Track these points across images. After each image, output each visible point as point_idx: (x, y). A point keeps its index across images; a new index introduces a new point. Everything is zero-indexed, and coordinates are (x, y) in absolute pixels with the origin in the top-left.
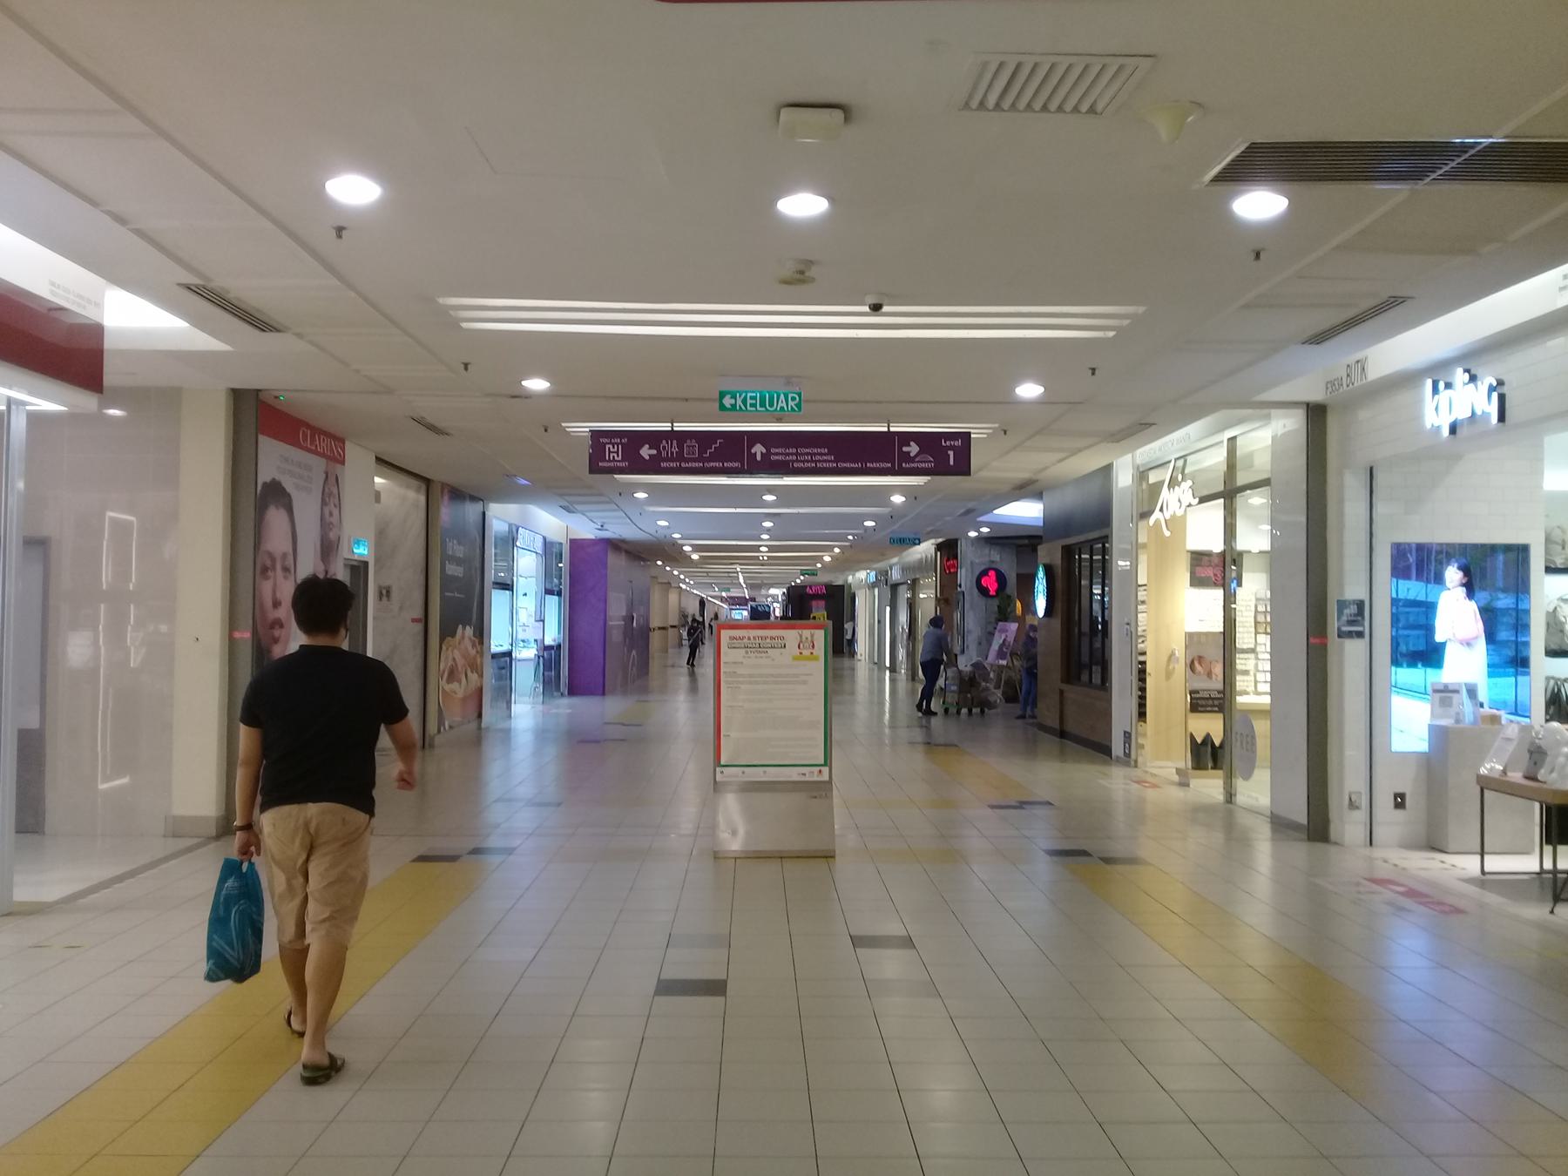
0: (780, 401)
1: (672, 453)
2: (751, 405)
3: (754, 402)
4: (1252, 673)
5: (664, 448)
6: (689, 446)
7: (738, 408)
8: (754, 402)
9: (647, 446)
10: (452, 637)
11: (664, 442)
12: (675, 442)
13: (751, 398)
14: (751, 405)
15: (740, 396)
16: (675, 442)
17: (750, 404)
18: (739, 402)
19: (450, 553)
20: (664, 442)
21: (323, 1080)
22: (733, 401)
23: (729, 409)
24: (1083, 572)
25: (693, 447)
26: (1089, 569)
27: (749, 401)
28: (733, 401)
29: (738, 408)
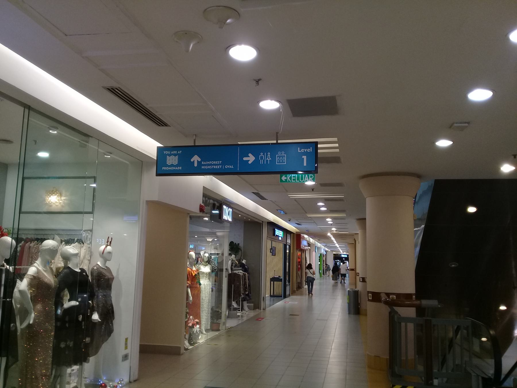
0: (306, 178)
1: (267, 161)
2: (294, 180)
3: (295, 178)
4: (241, 312)
5: (262, 158)
6: (280, 157)
7: (288, 181)
8: (295, 178)
9: (250, 162)
10: (271, 278)
11: (262, 154)
12: (269, 154)
13: (294, 177)
14: (294, 180)
15: (289, 176)
16: (269, 154)
17: (293, 179)
18: (288, 178)
19: (61, 296)
20: (262, 154)
21: (245, 281)
22: (286, 178)
23: (284, 182)
24: (17, 230)
25: (283, 157)
26: (17, 234)
27: (292, 178)
28: (286, 178)
29: (288, 181)
